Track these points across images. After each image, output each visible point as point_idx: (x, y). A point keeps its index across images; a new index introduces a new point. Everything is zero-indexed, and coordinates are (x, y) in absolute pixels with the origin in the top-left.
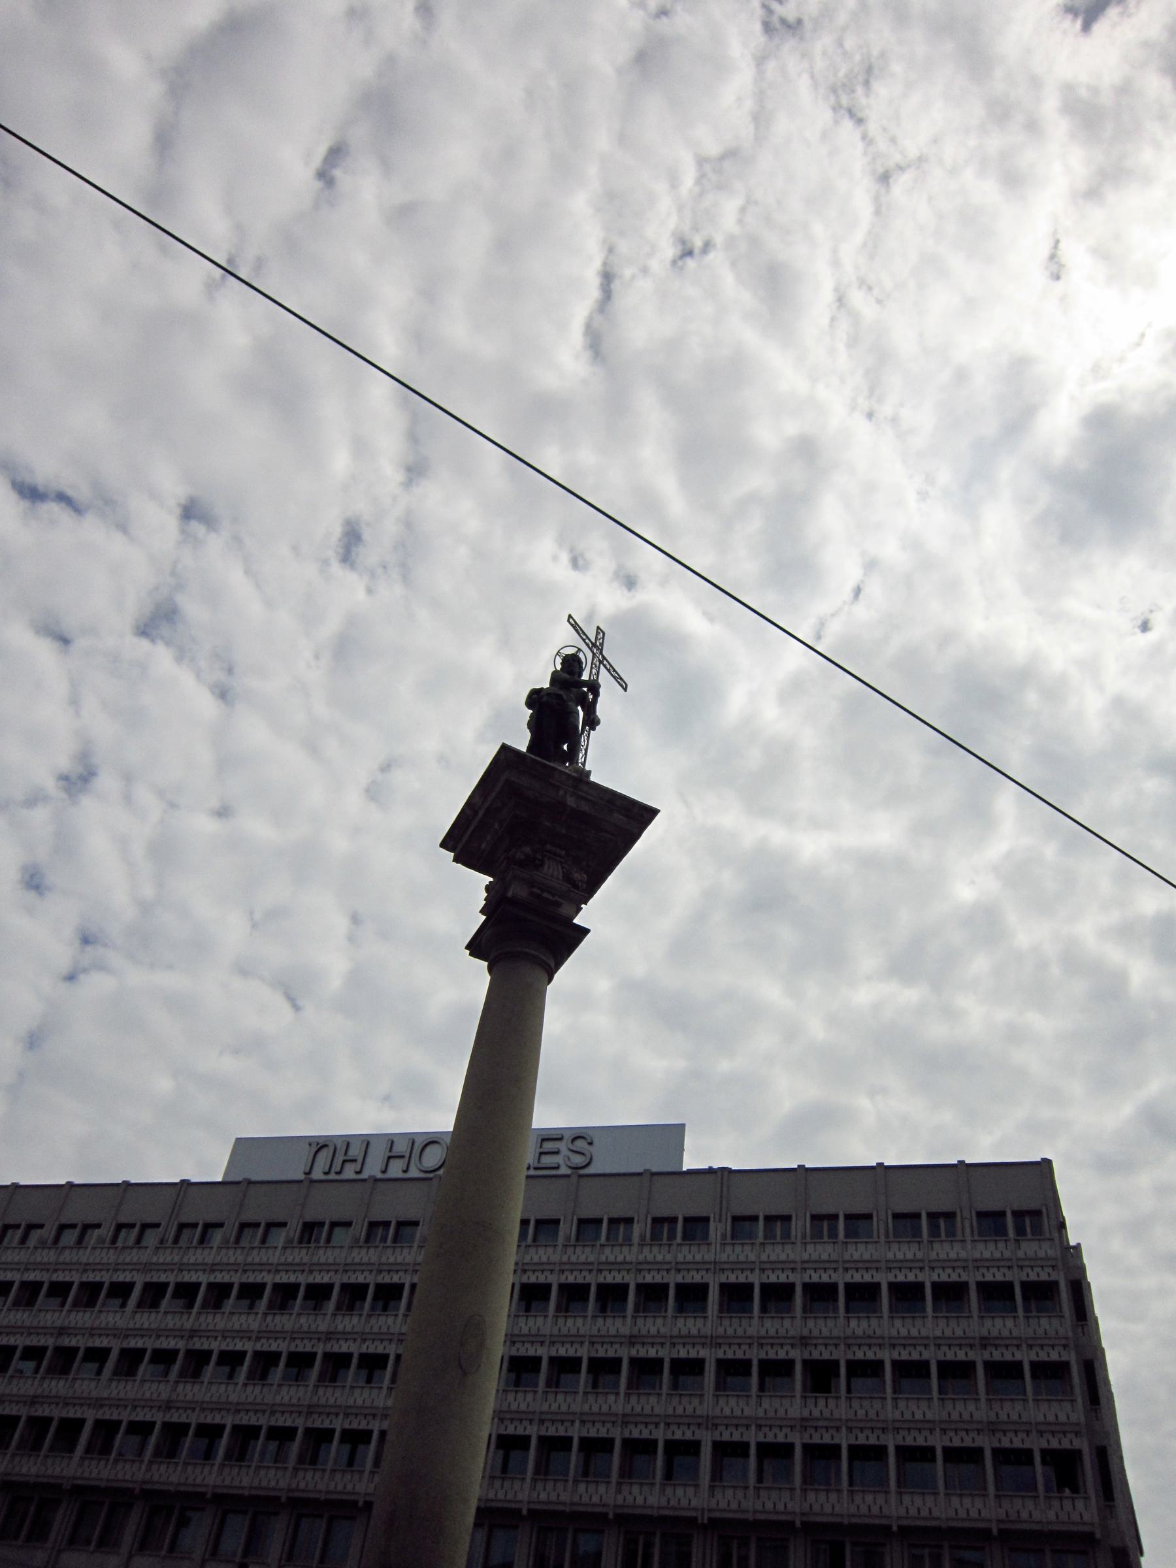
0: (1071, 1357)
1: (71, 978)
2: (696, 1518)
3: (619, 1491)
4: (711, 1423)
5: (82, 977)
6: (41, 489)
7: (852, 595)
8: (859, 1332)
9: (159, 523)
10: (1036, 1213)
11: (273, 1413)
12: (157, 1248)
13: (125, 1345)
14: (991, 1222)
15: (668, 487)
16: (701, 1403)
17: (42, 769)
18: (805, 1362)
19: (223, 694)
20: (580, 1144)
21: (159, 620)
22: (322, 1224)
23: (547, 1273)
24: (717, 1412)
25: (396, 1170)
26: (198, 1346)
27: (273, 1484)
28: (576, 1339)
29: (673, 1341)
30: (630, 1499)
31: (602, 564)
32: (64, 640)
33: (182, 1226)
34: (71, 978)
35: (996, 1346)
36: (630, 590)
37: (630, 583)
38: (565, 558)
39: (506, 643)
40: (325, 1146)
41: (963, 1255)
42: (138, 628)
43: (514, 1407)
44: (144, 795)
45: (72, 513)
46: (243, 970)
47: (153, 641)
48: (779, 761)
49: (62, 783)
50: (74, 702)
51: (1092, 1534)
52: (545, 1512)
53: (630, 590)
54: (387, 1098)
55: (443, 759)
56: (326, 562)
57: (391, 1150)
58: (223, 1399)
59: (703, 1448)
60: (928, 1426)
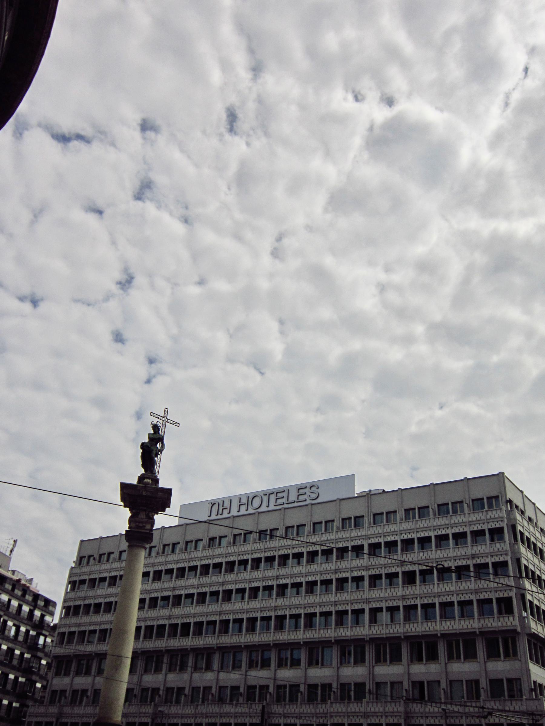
0: (508, 559)
1: (148, 381)
2: (364, 639)
3: (335, 631)
4: (367, 601)
5: (154, 380)
6: (67, 135)
7: (524, 73)
8: (423, 558)
9: (131, 136)
10: (497, 497)
11: (207, 616)
12: (156, 556)
13: (151, 596)
14: (478, 504)
15: (402, 39)
16: (364, 594)
17: (108, 281)
18: (403, 573)
19: (186, 221)
20: (314, 489)
21: (144, 190)
22: (216, 538)
23: (302, 548)
24: (370, 596)
25: (243, 511)
26: (177, 593)
27: (211, 642)
28: (315, 573)
29: (352, 570)
30: (340, 634)
31: (372, 95)
32: (100, 212)
33: (164, 546)
34: (148, 381)
35: (478, 557)
36: (390, 106)
37: (390, 102)
38: (350, 97)
39: (328, 154)
40: (215, 504)
41: (464, 520)
42: (135, 196)
43: (294, 603)
44: (160, 283)
45: (86, 144)
46: (231, 359)
47: (144, 202)
48: (496, 182)
49: (118, 286)
50: (114, 243)
51: (515, 630)
52: (309, 642)
53: (390, 106)
54: (318, 410)
55: (309, 228)
56: (221, 135)
57: (240, 502)
58: (189, 613)
59: (366, 611)
60: (451, 593)
